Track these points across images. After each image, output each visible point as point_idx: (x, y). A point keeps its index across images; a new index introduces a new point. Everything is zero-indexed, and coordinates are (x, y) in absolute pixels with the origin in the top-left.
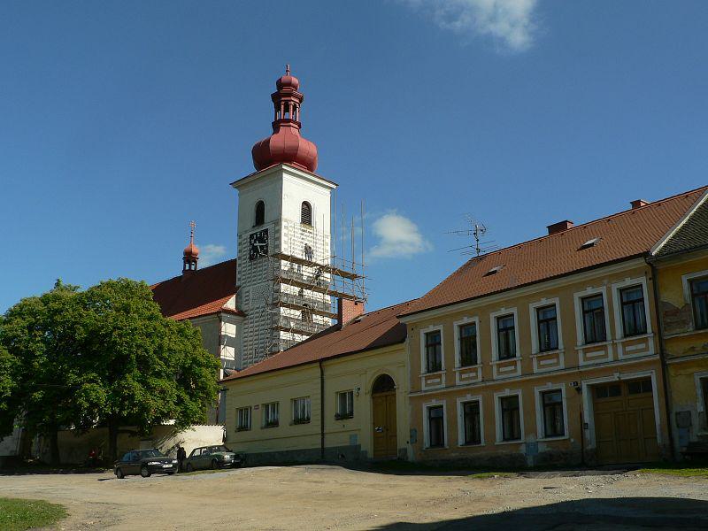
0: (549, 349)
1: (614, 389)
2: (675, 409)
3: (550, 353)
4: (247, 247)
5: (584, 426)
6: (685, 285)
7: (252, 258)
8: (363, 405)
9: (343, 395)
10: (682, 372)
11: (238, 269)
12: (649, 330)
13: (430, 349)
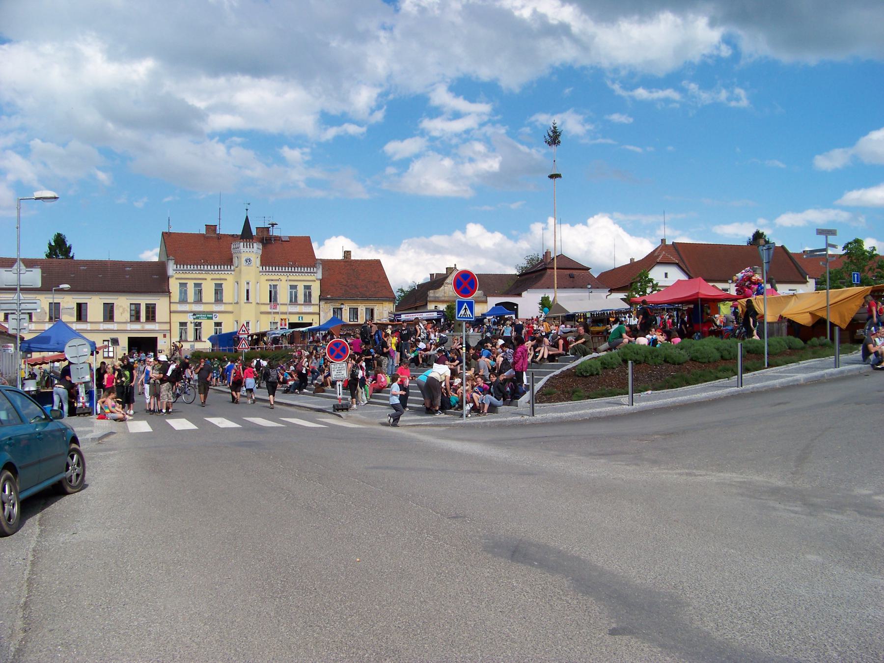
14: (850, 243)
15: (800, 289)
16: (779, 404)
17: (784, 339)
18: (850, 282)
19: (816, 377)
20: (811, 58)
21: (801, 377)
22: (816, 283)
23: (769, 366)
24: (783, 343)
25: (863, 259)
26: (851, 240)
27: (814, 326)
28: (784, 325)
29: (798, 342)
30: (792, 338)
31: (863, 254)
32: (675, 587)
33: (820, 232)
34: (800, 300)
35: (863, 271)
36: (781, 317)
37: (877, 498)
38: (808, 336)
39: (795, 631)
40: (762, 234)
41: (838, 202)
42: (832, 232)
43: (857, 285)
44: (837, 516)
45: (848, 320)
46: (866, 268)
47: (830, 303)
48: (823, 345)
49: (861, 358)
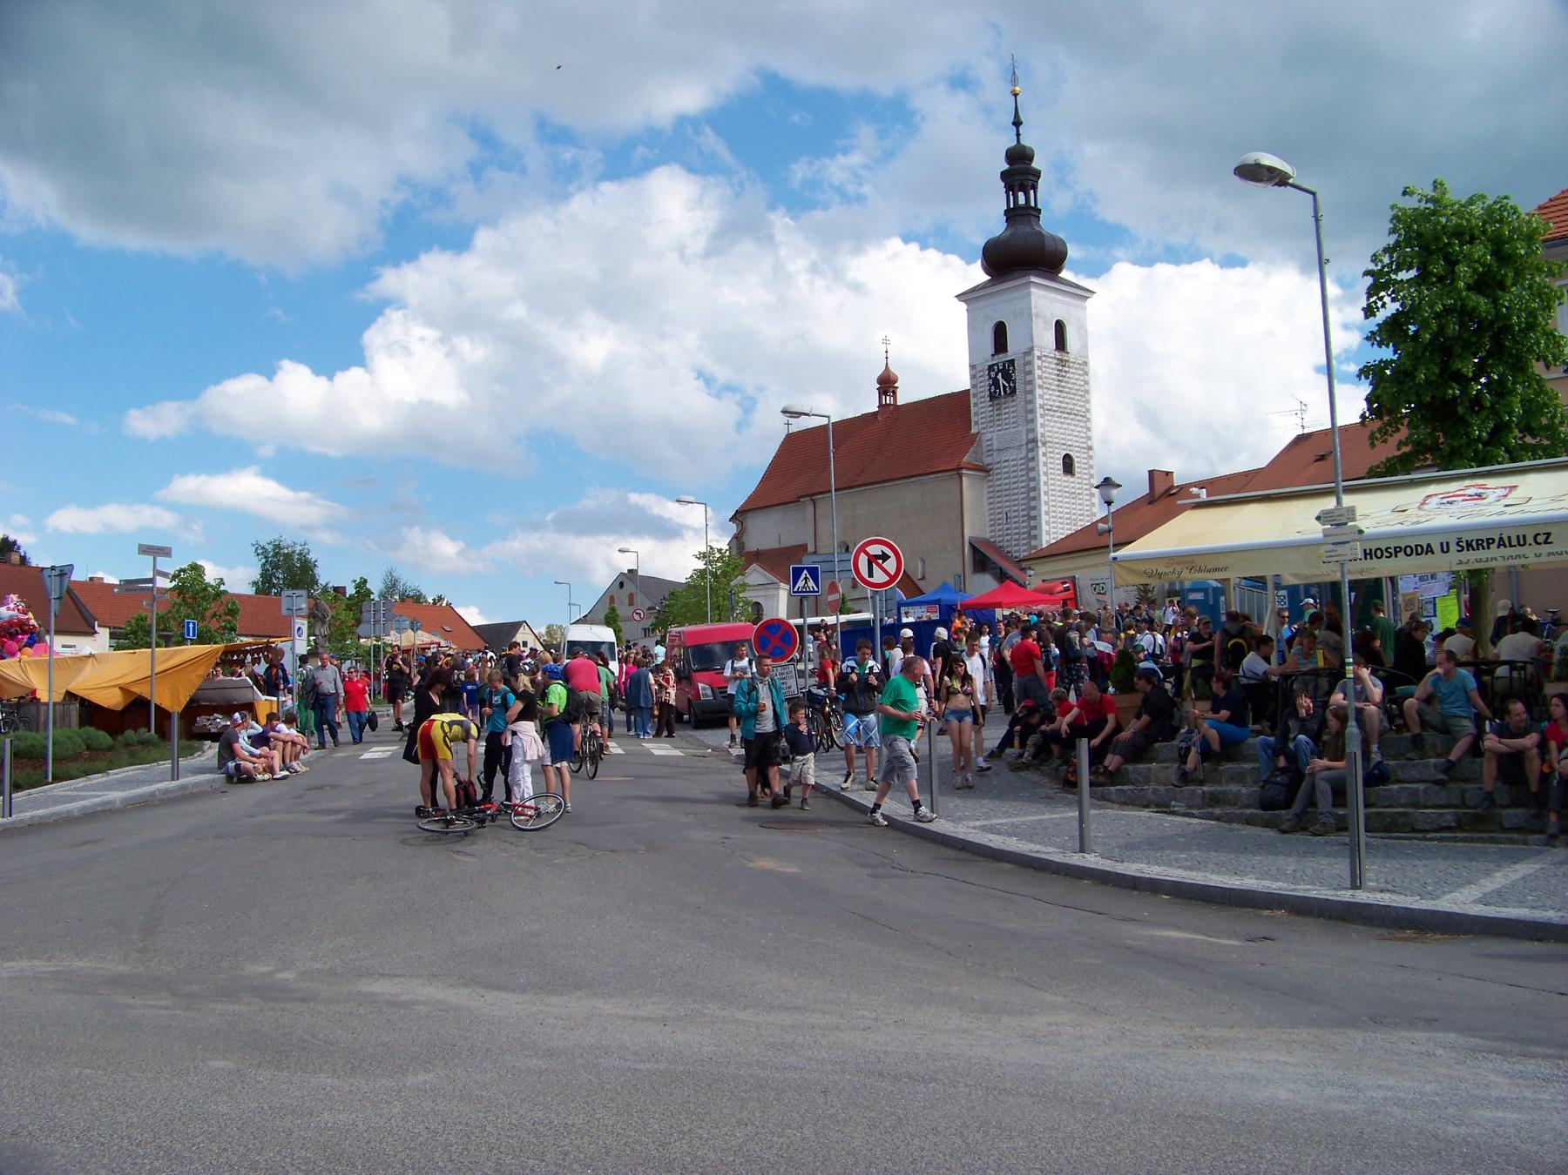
4: (1018, 376)
7: (992, 397)
11: (973, 400)
14: (183, 570)
15: (85, 646)
16: (85, 843)
17: (75, 733)
18: (182, 635)
19: (142, 796)
20: (133, 240)
21: (116, 796)
22: (112, 636)
23: (57, 779)
24: (79, 740)
25: (204, 598)
26: (185, 566)
27: (127, 709)
28: (75, 707)
29: (103, 737)
30: (91, 729)
31: (205, 589)
32: (14, 1134)
33: (145, 550)
34: (96, 665)
35: (203, 619)
36: (70, 695)
37: (281, 976)
38: (123, 727)
39: (235, 1159)
40: (15, 543)
41: (163, 494)
42: (165, 552)
43: (193, 642)
44: (231, 1007)
45: (184, 701)
46: (208, 614)
47: (158, 669)
48: (144, 743)
49: (215, 762)
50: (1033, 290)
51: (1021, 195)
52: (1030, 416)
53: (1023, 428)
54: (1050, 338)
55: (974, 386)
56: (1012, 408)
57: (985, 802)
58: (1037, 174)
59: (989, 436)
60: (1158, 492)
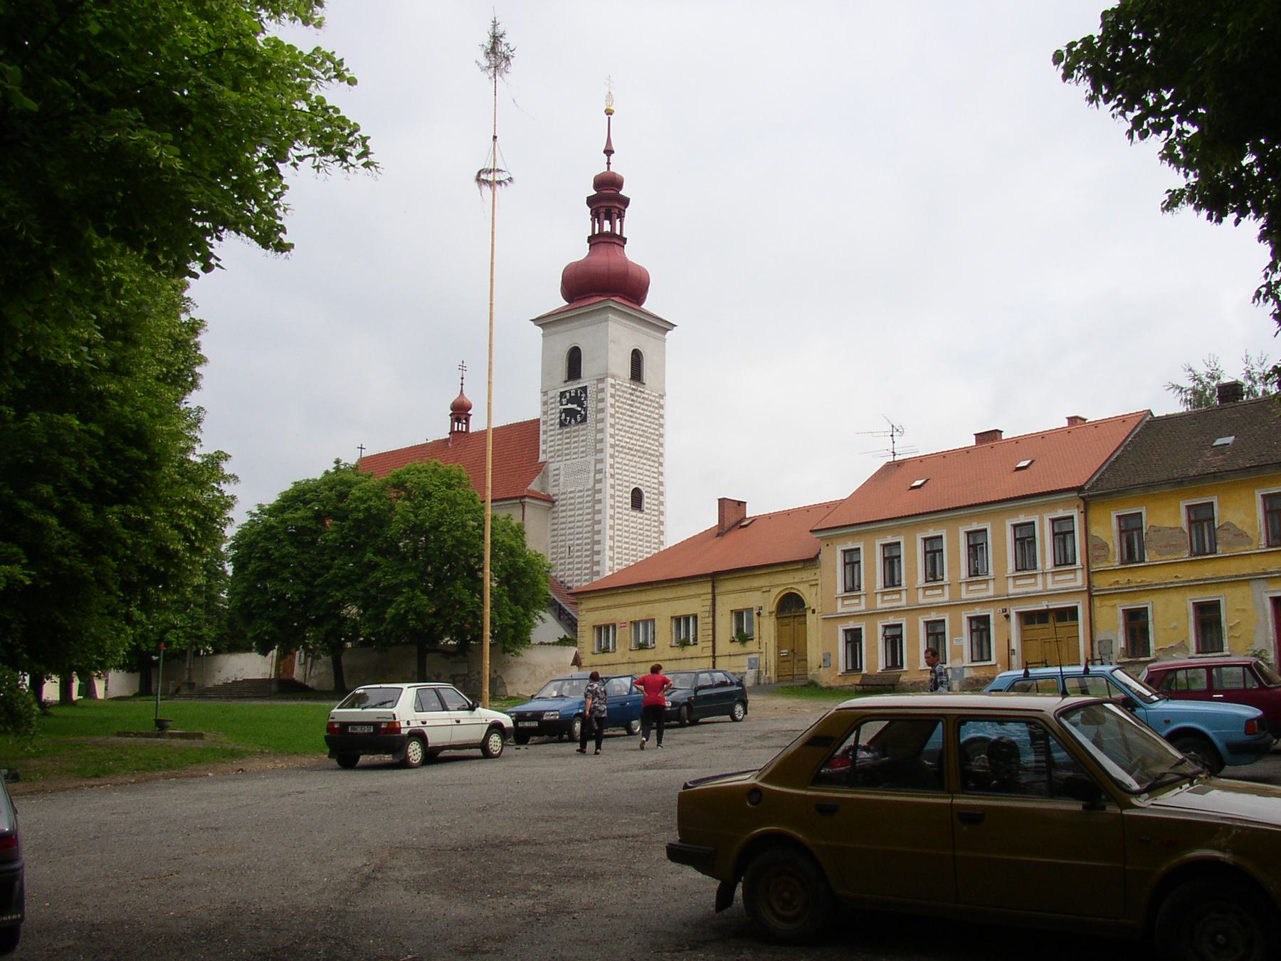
0: (852, 590)
1: (1042, 616)
2: (1097, 639)
3: (1068, 568)
4: (590, 404)
5: (1011, 652)
6: (1183, 511)
8: (767, 629)
9: (739, 614)
10: (1107, 603)
11: (542, 428)
12: (1078, 559)
13: (848, 567)
50: (610, 323)
51: (607, 223)
52: (599, 446)
53: (591, 459)
54: (623, 368)
55: (545, 413)
56: (584, 433)
57: (312, 901)
58: (625, 202)
59: (556, 465)
60: (727, 524)
